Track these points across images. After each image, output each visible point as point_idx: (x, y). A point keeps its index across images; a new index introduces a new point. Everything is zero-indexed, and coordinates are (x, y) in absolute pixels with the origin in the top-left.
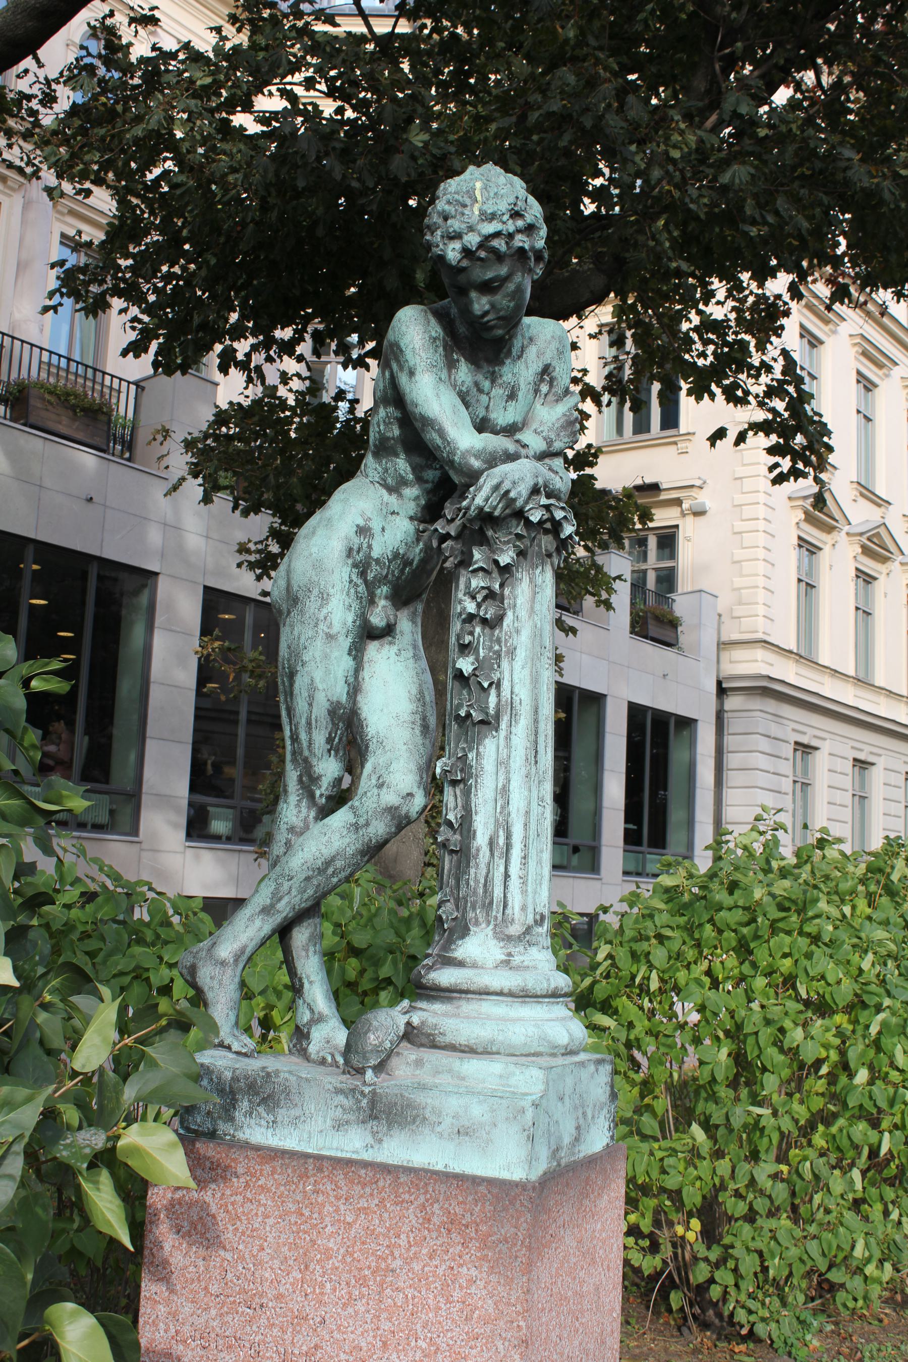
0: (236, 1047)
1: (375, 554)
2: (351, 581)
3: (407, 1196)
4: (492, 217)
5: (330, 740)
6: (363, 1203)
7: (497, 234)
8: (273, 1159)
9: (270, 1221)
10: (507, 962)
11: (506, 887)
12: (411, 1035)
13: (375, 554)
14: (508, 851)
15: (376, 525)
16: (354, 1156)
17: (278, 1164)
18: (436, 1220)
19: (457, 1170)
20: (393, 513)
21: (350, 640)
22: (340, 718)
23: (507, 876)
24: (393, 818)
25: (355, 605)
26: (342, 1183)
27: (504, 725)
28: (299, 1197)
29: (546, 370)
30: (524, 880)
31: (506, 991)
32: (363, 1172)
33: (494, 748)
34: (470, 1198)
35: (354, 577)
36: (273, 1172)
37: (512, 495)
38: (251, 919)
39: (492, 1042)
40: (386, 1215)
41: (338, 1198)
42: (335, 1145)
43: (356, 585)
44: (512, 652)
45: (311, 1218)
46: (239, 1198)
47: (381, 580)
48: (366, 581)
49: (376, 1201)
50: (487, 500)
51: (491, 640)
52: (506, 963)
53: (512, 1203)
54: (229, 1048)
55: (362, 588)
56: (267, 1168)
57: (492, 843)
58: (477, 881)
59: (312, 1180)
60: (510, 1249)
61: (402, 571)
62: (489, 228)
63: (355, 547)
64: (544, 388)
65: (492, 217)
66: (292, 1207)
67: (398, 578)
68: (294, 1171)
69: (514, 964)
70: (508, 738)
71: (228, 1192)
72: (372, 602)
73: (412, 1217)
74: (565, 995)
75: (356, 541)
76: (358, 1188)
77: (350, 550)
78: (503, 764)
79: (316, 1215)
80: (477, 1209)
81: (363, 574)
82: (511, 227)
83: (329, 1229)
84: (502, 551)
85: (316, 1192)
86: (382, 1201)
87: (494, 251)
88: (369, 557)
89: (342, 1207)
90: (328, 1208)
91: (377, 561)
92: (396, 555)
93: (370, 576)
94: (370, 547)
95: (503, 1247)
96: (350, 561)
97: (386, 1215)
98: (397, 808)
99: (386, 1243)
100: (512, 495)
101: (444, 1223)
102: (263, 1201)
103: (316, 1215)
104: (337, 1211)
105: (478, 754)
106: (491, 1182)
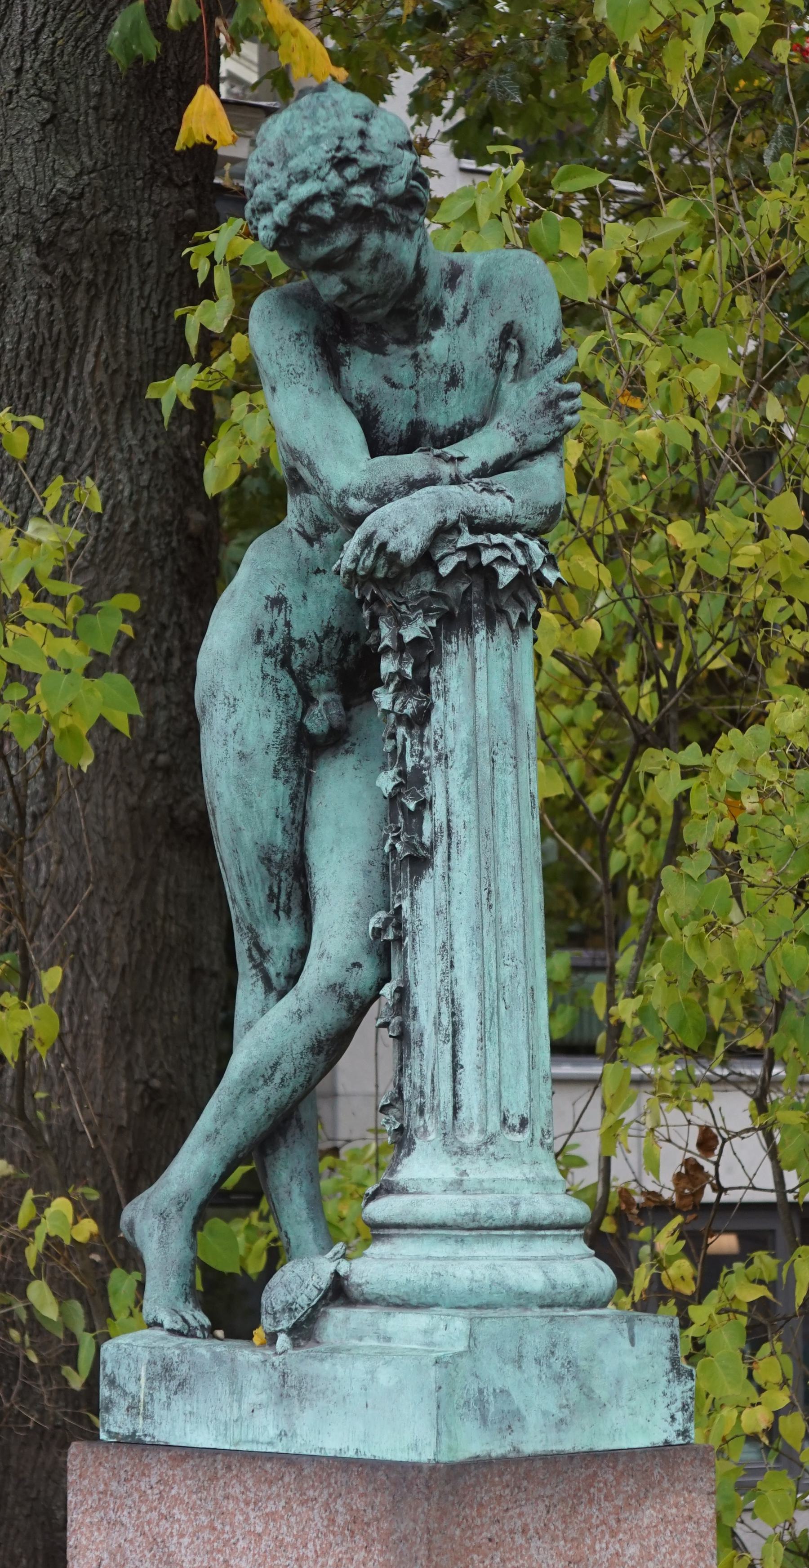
0: (167, 1325)
1: (296, 634)
2: (265, 676)
3: (311, 1493)
4: (304, 176)
5: (272, 897)
6: (271, 1507)
7: (317, 198)
8: (184, 1459)
9: (186, 1541)
10: (460, 1183)
11: (455, 1080)
12: (338, 1292)
13: (296, 634)
14: (455, 1033)
15: (291, 593)
16: (270, 1449)
17: (188, 1465)
18: (340, 1520)
19: (369, 1456)
20: (318, 571)
21: (273, 756)
22: (280, 866)
23: (456, 1066)
24: (340, 999)
25: (277, 708)
26: (250, 1483)
27: (439, 858)
28: (210, 1506)
29: (508, 332)
30: (482, 1068)
31: (450, 1222)
32: (268, 1466)
33: (430, 892)
34: (370, 1488)
35: (269, 670)
36: (186, 1478)
37: (391, 548)
38: (193, 1153)
39: (425, 1289)
40: (293, 1519)
41: (247, 1504)
42: (250, 1437)
43: (275, 680)
44: (443, 758)
45: (223, 1532)
46: (155, 1515)
47: (317, 666)
48: (291, 672)
49: (283, 1503)
50: (356, 560)
51: (421, 743)
52: (458, 1185)
53: (409, 1490)
54: (161, 1325)
55: (286, 682)
56: (179, 1472)
57: (437, 1024)
58: (422, 1076)
59: (222, 1482)
60: (410, 1549)
61: (345, 650)
62: (301, 192)
63: (267, 629)
64: (512, 358)
65: (304, 176)
66: (204, 1519)
67: (340, 661)
68: (205, 1473)
69: (466, 1185)
70: (447, 877)
71: (144, 1509)
72: (307, 699)
73: (317, 1519)
74: (577, 1226)
75: (266, 620)
76: (265, 1487)
77: (260, 633)
78: (443, 912)
79: (227, 1528)
80: (377, 1501)
81: (285, 663)
82: (334, 180)
83: (242, 1544)
84: (409, 621)
85: (227, 1497)
86: (289, 1501)
87: (316, 220)
88: (288, 639)
89: (252, 1515)
90: (240, 1517)
91: (302, 643)
92: (328, 631)
93: (296, 666)
94: (288, 624)
95: (404, 1547)
96: (260, 649)
97: (293, 1519)
98: (341, 986)
99: (295, 1556)
100: (391, 548)
101: (347, 1523)
102: (177, 1516)
103: (227, 1528)
104: (247, 1520)
105: (413, 903)
106: (390, 1466)
